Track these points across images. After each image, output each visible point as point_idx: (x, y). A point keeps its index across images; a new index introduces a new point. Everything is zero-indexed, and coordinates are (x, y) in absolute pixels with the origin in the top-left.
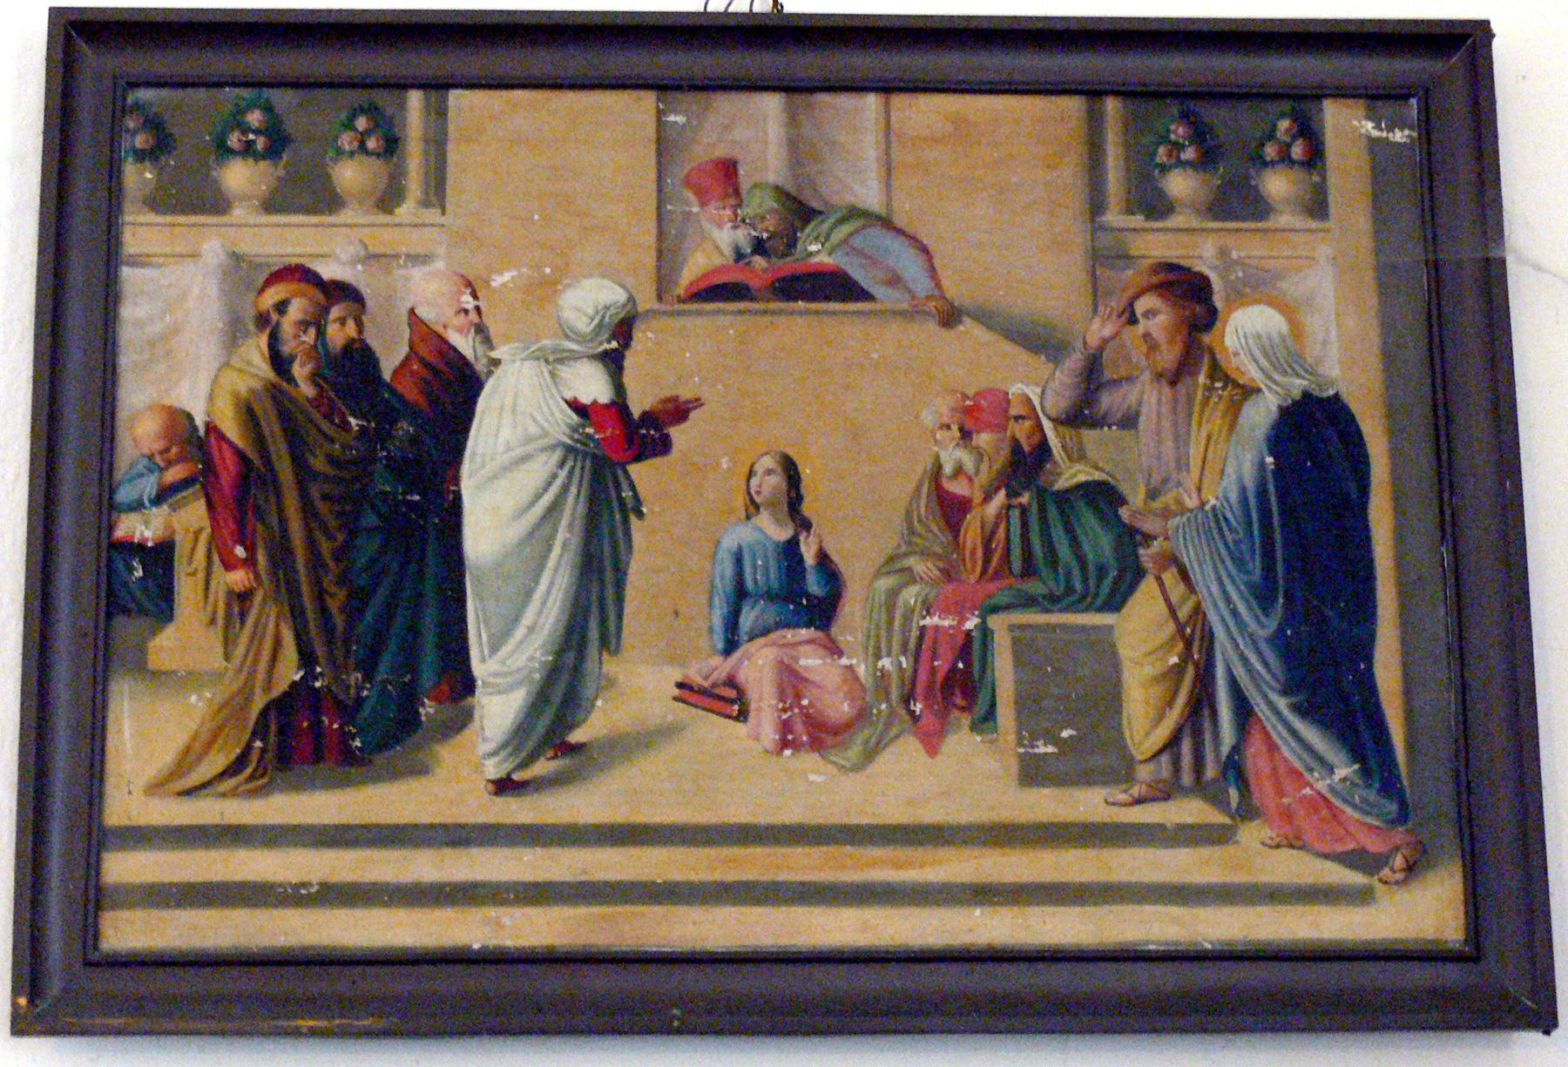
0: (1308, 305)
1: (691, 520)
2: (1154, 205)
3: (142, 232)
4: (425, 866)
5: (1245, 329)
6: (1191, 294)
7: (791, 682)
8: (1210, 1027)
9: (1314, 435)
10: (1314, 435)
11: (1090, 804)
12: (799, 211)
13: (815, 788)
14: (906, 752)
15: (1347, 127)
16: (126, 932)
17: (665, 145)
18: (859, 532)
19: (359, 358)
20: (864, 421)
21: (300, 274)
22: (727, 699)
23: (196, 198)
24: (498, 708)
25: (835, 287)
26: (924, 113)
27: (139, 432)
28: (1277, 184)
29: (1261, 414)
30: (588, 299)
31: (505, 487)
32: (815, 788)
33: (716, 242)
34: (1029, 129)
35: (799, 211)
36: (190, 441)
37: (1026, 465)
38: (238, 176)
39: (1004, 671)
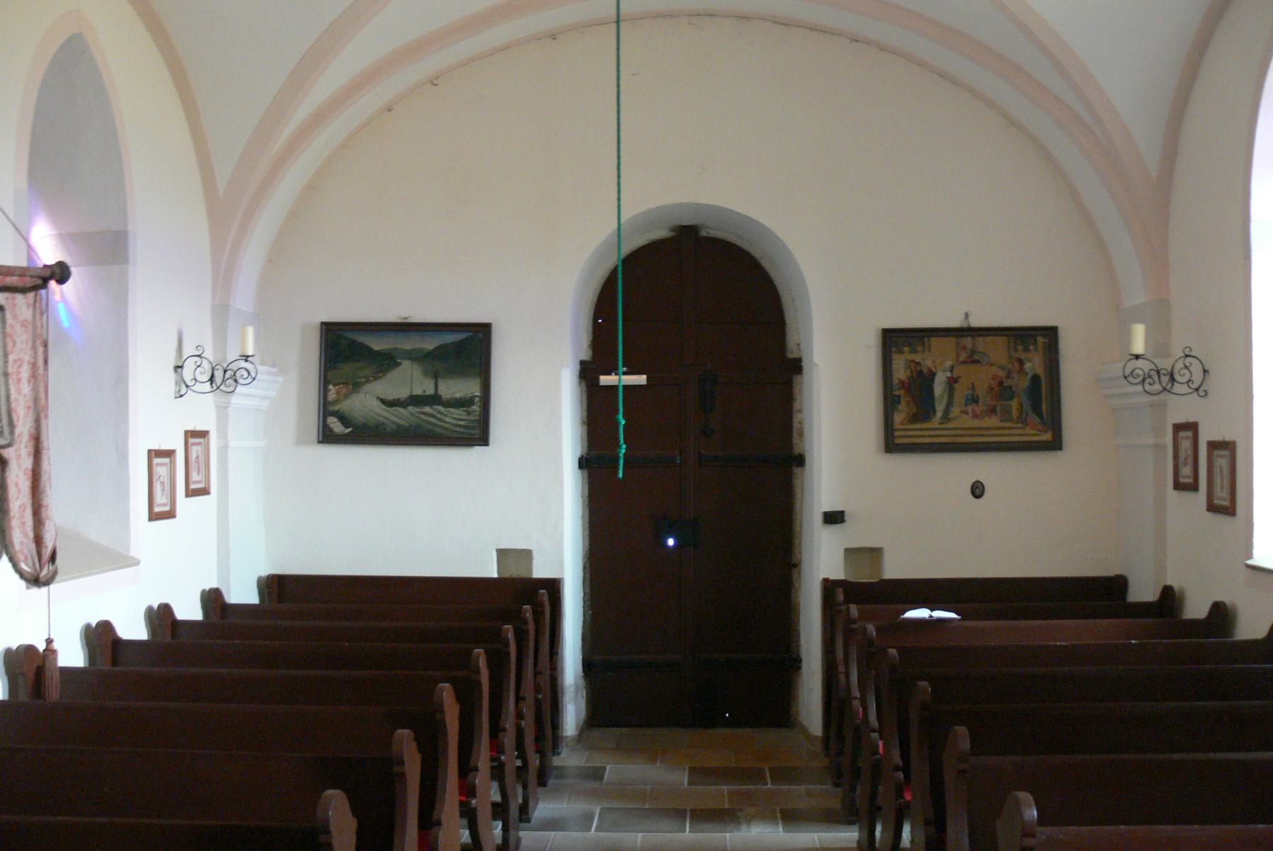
0: (1034, 364)
1: (961, 391)
2: (1016, 350)
3: (895, 356)
4: (931, 433)
5: (1028, 366)
6: (1021, 362)
7: (974, 411)
8: (997, 351)
9: (1036, 379)
10: (1036, 379)
11: (1009, 424)
12: (973, 352)
13: (976, 423)
14: (986, 419)
15: (1040, 340)
16: (897, 441)
17: (957, 344)
18: (980, 392)
19: (921, 372)
20: (982, 378)
21: (913, 361)
22: (966, 413)
23: (901, 352)
24: (939, 414)
25: (977, 362)
26: (988, 339)
27: (896, 381)
28: (1032, 348)
29: (1029, 376)
30: (948, 364)
31: (939, 387)
32: (976, 423)
33: (963, 356)
34: (1001, 340)
35: (973, 352)
36: (901, 382)
37: (1001, 383)
38: (906, 349)
39: (998, 409)
